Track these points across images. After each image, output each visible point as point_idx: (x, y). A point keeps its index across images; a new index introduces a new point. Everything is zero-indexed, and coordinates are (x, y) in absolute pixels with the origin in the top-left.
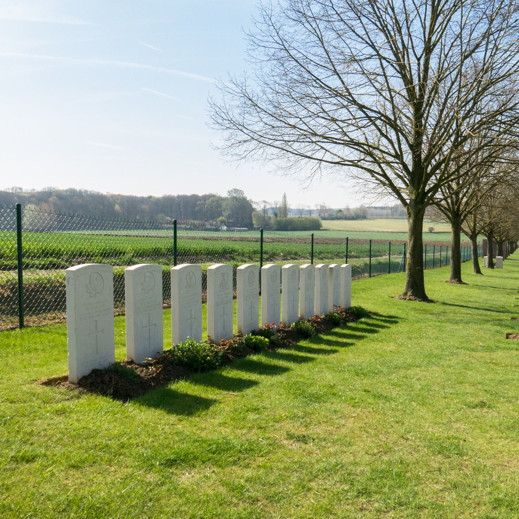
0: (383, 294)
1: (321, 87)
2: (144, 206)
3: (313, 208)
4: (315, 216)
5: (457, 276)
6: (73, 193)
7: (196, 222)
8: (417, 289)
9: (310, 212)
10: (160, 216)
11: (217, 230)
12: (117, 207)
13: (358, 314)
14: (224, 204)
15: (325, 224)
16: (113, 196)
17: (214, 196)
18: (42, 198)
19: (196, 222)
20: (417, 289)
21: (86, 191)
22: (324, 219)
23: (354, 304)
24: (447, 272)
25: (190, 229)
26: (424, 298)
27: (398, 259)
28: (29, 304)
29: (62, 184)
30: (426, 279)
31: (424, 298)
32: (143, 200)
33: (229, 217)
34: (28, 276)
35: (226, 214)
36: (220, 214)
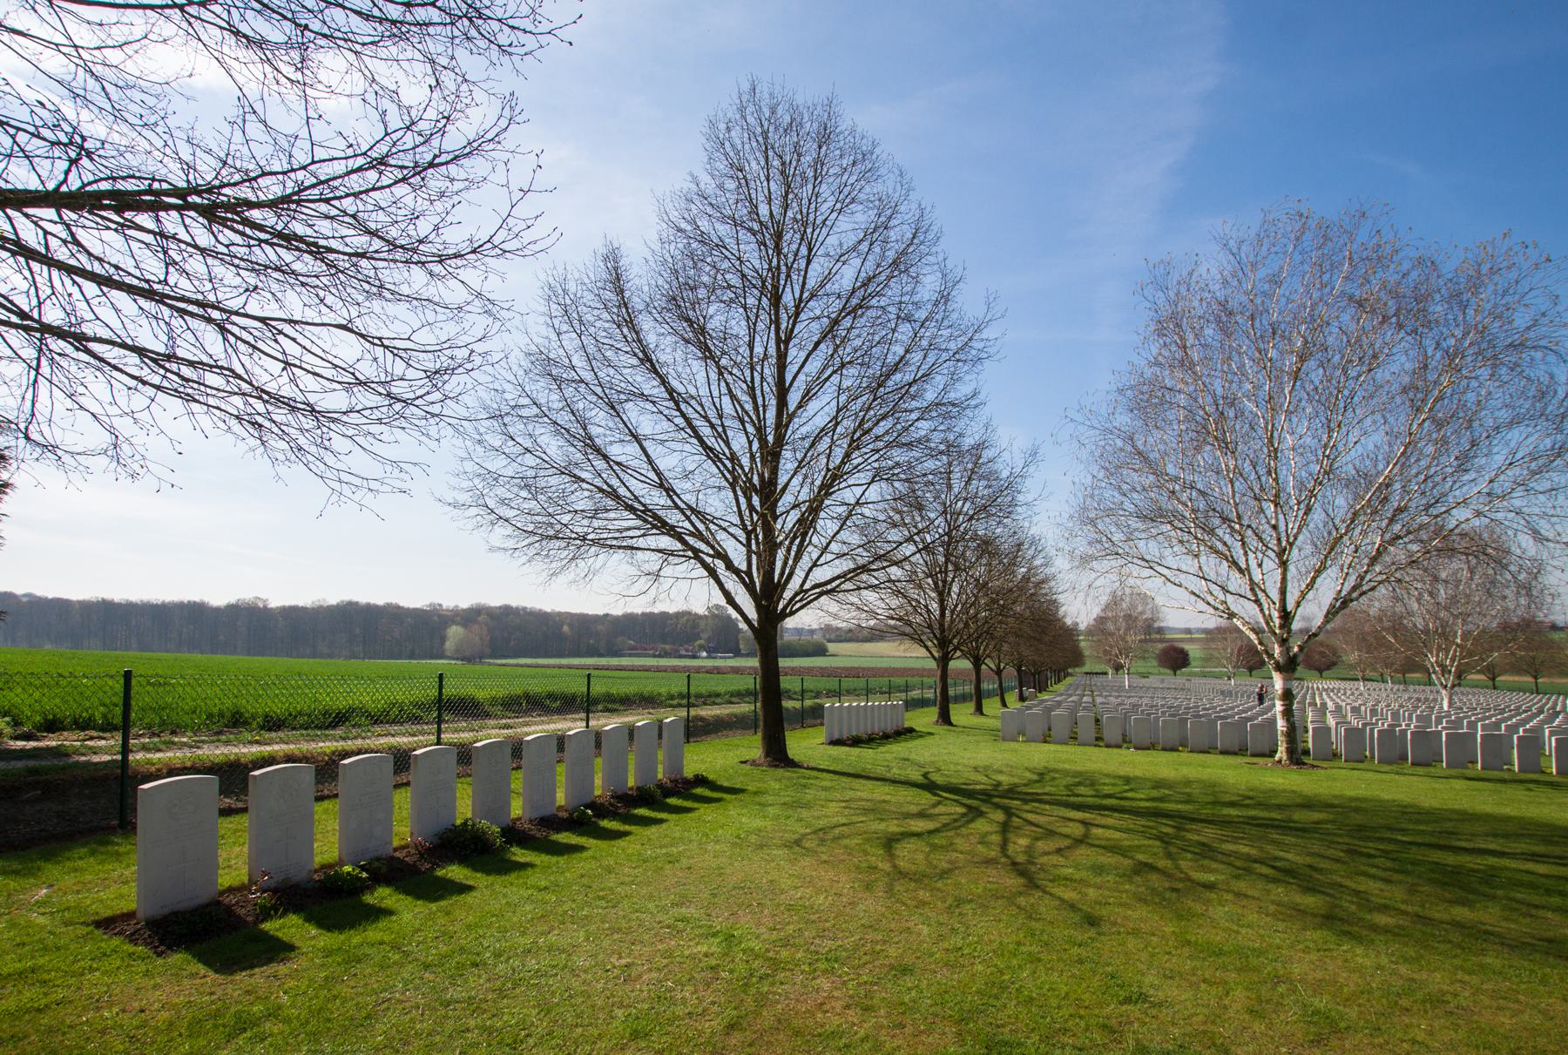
0: (924, 719)
1: (753, 389)
2: (600, 627)
3: (815, 626)
4: (817, 637)
5: (979, 710)
6: (507, 610)
7: (667, 647)
8: (945, 718)
9: (812, 632)
10: (620, 639)
11: (694, 657)
12: (566, 628)
13: (911, 730)
14: (702, 624)
15: (832, 647)
16: (560, 614)
17: (689, 613)
18: (470, 617)
19: (667, 647)
20: (945, 718)
21: (525, 609)
22: (830, 641)
23: (907, 725)
24: (971, 706)
25: (660, 656)
26: (951, 724)
27: (929, 694)
28: (92, 808)
29: (495, 601)
30: (952, 713)
31: (951, 724)
32: (596, 619)
33: (709, 640)
34: (693, 712)
35: (705, 636)
36: (697, 637)
